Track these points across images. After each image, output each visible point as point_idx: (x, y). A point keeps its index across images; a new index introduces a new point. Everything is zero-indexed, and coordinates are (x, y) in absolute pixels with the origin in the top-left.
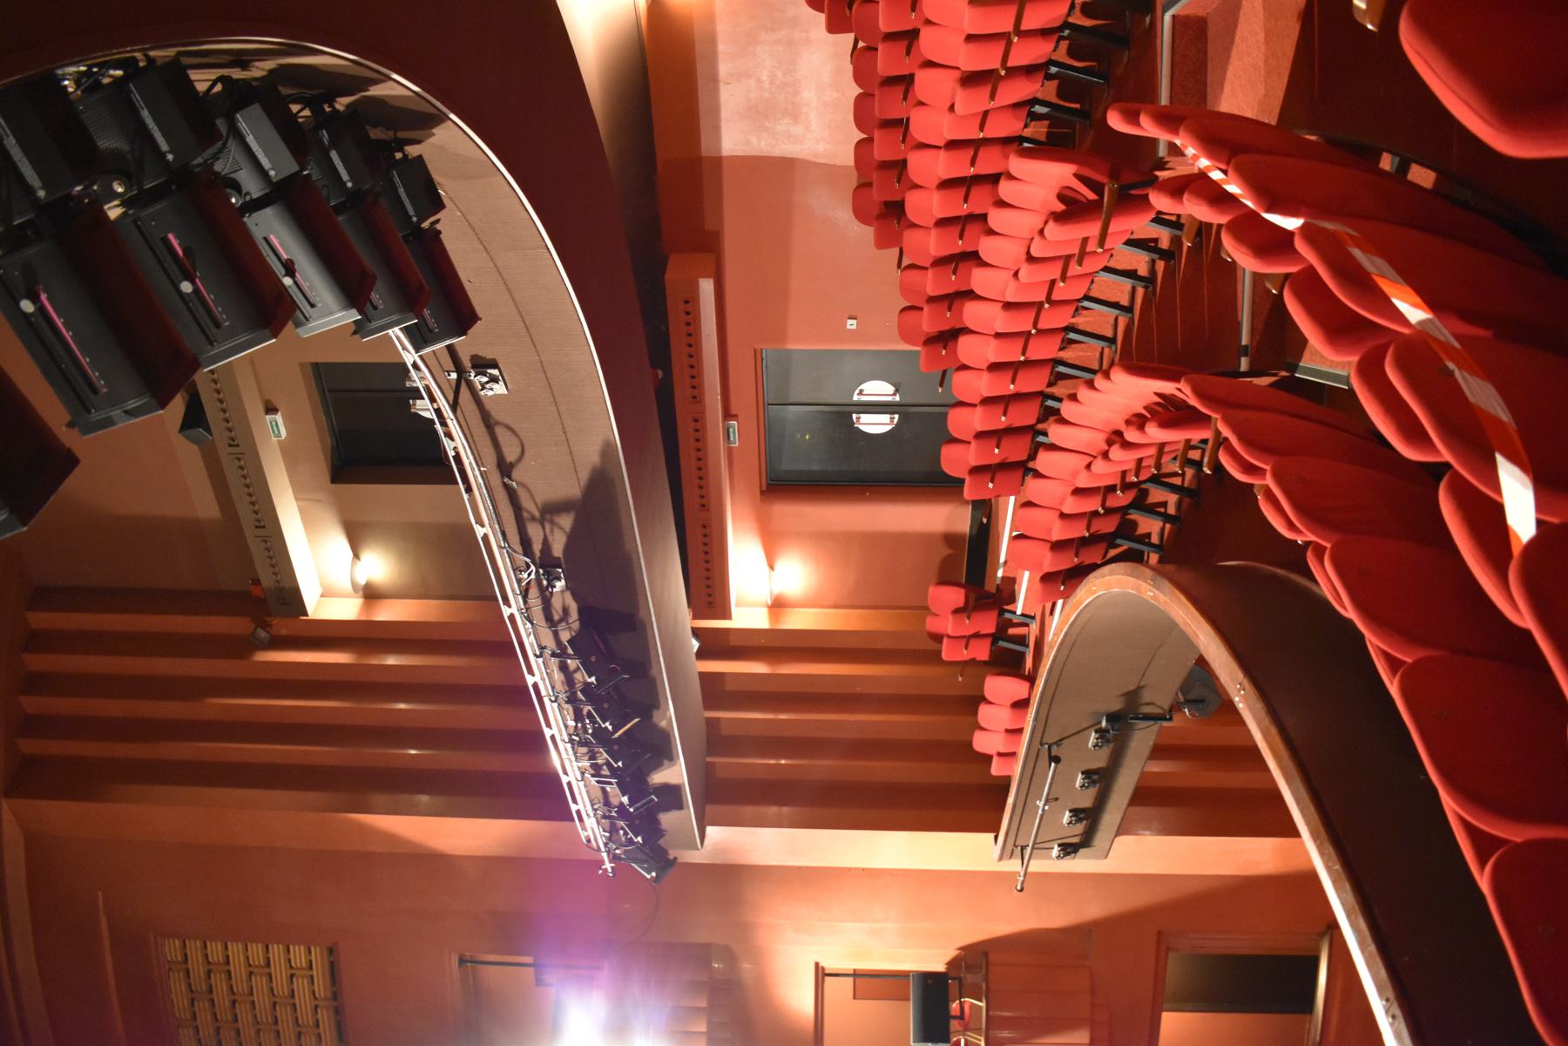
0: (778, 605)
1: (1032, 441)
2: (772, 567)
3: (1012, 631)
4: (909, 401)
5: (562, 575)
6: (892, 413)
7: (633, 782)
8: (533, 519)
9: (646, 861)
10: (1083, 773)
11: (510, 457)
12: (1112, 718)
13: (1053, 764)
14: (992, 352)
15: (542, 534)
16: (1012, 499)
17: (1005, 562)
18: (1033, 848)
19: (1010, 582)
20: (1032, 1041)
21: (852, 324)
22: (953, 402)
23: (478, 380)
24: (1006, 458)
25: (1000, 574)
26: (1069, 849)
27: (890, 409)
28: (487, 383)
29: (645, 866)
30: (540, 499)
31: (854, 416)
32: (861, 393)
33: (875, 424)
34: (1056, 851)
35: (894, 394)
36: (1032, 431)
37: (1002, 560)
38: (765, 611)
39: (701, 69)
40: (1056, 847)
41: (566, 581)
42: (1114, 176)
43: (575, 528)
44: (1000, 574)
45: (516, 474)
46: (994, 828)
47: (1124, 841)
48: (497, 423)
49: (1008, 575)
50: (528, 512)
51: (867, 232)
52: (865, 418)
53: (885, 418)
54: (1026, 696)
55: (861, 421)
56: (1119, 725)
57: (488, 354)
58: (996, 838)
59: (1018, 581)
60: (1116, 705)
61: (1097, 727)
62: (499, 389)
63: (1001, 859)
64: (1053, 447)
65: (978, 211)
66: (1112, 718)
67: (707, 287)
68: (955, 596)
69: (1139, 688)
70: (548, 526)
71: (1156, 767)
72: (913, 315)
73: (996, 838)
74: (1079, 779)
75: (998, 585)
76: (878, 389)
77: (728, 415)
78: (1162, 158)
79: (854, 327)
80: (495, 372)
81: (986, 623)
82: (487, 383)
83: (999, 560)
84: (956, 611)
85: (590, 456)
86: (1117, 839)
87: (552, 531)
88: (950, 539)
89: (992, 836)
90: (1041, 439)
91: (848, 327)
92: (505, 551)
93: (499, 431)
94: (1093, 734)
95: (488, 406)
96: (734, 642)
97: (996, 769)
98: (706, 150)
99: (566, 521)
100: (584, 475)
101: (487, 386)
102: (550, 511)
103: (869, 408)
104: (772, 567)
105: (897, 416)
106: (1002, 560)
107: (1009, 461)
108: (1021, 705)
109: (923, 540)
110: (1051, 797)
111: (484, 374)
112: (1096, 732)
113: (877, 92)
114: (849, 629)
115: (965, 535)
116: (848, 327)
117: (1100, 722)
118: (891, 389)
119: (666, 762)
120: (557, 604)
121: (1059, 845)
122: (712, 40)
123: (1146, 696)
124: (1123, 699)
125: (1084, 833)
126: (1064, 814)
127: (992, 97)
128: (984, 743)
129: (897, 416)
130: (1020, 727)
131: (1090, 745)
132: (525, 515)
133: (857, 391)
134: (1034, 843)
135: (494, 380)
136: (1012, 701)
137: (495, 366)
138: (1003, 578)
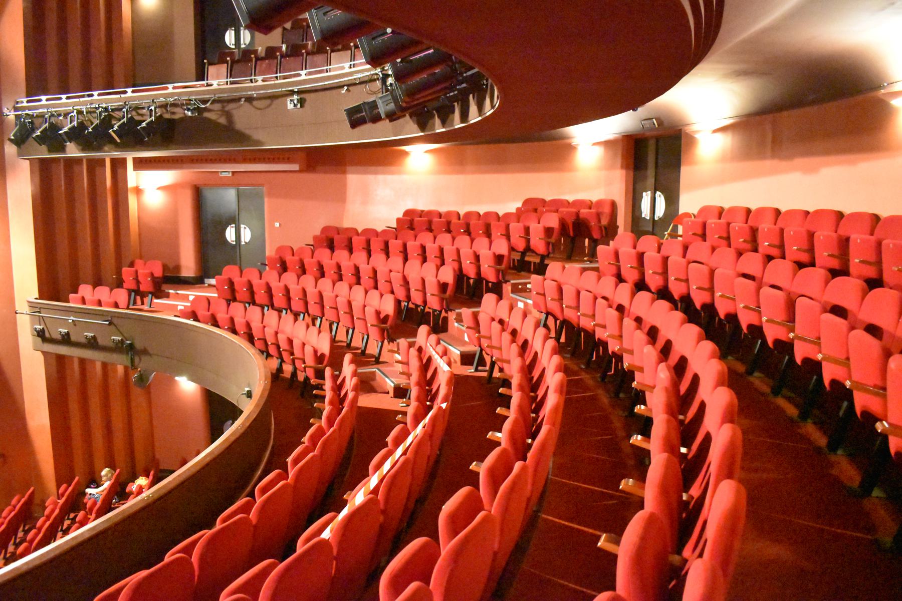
0: (138, 191)
1: (301, 312)
2: (159, 189)
3: (138, 298)
4: (242, 248)
5: (194, 115)
6: (236, 241)
7: (78, 134)
8: (223, 107)
9: (21, 134)
10: (94, 335)
11: (255, 103)
12: (131, 346)
13: (108, 323)
14: (328, 295)
15: (216, 109)
16: (216, 295)
17: (178, 293)
18: (39, 316)
19: (167, 296)
20: (457, 347)
21: (277, 225)
22: (242, 268)
23: (295, 97)
24: (293, 300)
25: (171, 291)
26: (41, 334)
27: (238, 241)
28: (294, 103)
29: (18, 134)
30: (234, 112)
31: (234, 225)
32: (245, 228)
33: (230, 234)
34: (39, 327)
35: (245, 242)
36: (289, 307)
37: (179, 292)
38: (135, 185)
39: (380, 168)
40: (41, 327)
41: (190, 116)
42: (391, 327)
43: (219, 124)
44: (171, 291)
45: (247, 104)
46: (41, 297)
47: (40, 357)
48: (272, 101)
49: (171, 295)
50: (227, 105)
51: (318, 233)
52: (233, 230)
53: (234, 238)
54: (120, 307)
55: (232, 228)
56: (128, 349)
57: (306, 105)
58: (36, 299)
59: (168, 299)
60: (139, 345)
61: (124, 340)
62: (290, 106)
63: (28, 302)
64: (280, 317)
65: (362, 281)
66: (131, 346)
67: (296, 167)
68: (158, 273)
69: (150, 355)
70: (219, 112)
71: (98, 366)
72: (291, 253)
73: (36, 299)
74: (90, 335)
75: (164, 291)
76: (246, 235)
77: (233, 173)
78: (396, 341)
79: (276, 226)
80: (299, 106)
81: (146, 286)
82: (294, 103)
83: (178, 290)
84: (152, 274)
85: (257, 135)
86: (40, 352)
87: (217, 114)
88: (178, 268)
89: (38, 297)
90: (266, 308)
91: (276, 223)
92: (213, 96)
93: (268, 102)
94: (120, 338)
95: (284, 98)
96: (120, 171)
97: (72, 296)
98: (349, 168)
99: (223, 121)
100: (247, 132)
101: (292, 102)
102: (229, 115)
103: (237, 231)
104: (159, 189)
105: (234, 243)
106: (179, 292)
107: (255, 295)
108: (100, 303)
109: (176, 254)
110: (76, 323)
111: (298, 102)
112: (122, 339)
113: (379, 239)
114: (130, 225)
115: (181, 274)
116: (276, 223)
117: (127, 341)
118: (247, 241)
119: (80, 147)
120: (177, 110)
121: (43, 328)
122: (392, 173)
123: (144, 358)
124: (142, 348)
125: (52, 339)
126: (65, 329)
127: (432, 295)
128: (85, 290)
129: (234, 243)
130: (87, 303)
131: (113, 337)
132: (225, 104)
133: (245, 226)
134: (42, 316)
135: (295, 105)
136: (195, 310)
137: (301, 106)
138: (169, 293)
